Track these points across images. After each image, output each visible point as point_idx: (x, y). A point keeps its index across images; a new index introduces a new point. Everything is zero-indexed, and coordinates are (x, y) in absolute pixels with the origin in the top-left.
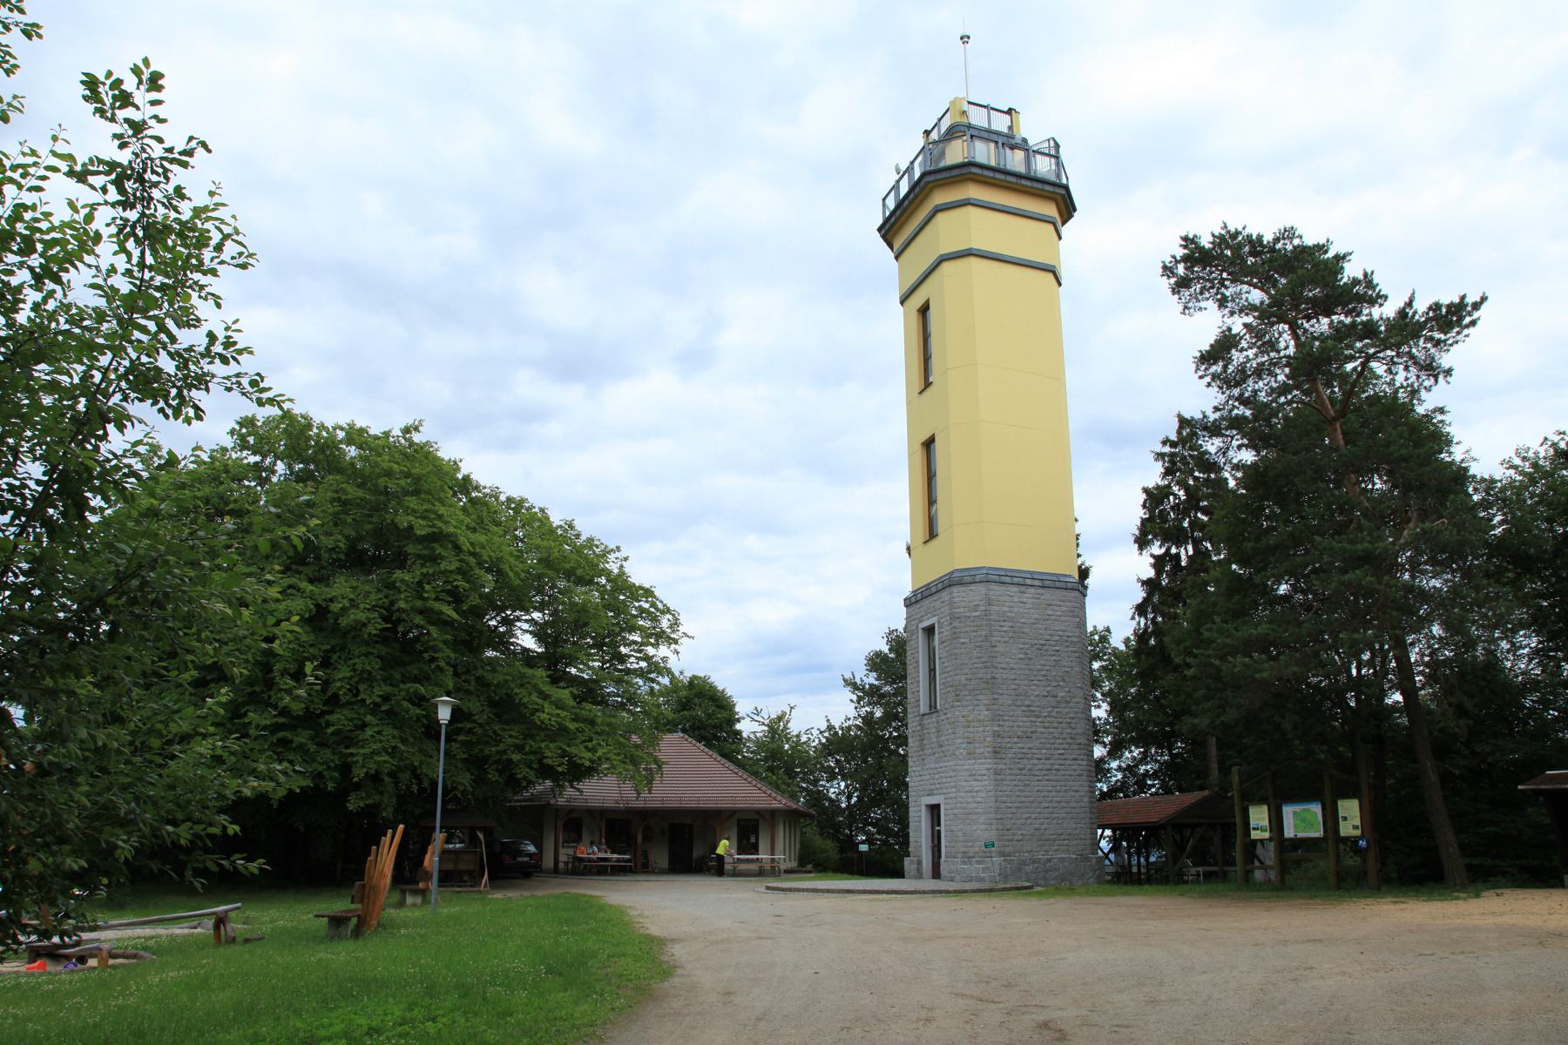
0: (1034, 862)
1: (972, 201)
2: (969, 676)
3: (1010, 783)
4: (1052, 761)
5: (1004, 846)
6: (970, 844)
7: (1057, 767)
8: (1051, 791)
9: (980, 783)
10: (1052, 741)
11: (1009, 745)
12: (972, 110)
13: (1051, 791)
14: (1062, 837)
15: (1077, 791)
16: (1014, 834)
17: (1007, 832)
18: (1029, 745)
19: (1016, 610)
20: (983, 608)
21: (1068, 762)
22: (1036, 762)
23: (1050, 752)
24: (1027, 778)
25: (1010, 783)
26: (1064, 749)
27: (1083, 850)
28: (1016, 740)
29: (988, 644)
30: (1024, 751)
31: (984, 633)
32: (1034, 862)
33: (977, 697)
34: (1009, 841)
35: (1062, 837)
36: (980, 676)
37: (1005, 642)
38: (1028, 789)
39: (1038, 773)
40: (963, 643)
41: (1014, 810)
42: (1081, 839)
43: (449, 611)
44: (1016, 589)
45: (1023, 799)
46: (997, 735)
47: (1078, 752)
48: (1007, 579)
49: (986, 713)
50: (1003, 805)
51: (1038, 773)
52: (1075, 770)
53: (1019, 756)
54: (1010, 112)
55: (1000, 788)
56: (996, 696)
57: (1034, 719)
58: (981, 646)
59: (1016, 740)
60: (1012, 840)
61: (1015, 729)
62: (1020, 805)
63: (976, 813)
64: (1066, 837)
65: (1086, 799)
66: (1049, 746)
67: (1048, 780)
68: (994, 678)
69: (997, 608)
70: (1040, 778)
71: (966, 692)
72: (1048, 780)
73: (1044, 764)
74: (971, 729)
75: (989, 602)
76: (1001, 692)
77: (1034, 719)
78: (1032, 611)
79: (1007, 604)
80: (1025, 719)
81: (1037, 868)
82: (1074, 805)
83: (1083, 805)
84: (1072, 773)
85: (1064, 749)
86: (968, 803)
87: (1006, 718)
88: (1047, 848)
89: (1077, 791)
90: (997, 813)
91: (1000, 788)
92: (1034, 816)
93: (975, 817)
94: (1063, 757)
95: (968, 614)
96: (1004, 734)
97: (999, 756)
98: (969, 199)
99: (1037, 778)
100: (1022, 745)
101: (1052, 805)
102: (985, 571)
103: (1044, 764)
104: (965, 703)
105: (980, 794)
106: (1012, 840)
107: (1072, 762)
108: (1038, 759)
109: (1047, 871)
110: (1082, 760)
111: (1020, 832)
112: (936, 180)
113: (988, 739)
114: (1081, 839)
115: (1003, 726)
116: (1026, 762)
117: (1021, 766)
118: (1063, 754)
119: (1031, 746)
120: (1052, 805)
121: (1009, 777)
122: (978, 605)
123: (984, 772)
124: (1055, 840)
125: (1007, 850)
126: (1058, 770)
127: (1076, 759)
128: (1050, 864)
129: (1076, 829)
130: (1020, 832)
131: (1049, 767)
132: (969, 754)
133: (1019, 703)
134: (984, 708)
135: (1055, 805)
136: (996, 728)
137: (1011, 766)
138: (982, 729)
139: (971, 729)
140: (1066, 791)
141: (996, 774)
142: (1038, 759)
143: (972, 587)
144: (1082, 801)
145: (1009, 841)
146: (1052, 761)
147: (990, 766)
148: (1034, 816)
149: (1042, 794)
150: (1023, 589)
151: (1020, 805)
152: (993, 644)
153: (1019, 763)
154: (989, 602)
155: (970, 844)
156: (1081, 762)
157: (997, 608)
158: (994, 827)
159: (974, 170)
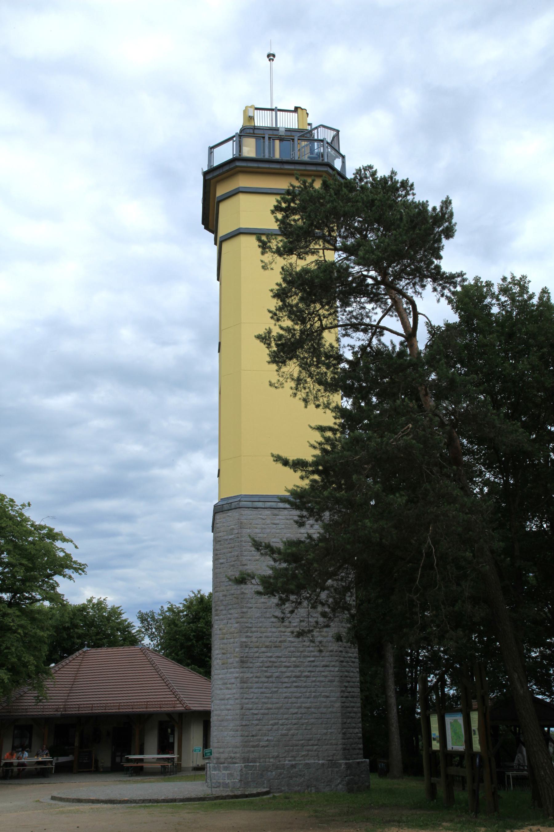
0: (277, 768)
1: (241, 190)
2: (225, 593)
3: (256, 691)
4: (302, 669)
5: (249, 752)
6: (221, 750)
7: (306, 674)
8: (299, 697)
9: (230, 691)
10: (301, 649)
11: (257, 655)
12: (257, 113)
13: (299, 697)
14: (311, 742)
15: (328, 697)
16: (260, 740)
17: (252, 739)
18: (277, 654)
19: (268, 530)
20: (236, 531)
21: (318, 669)
22: (284, 669)
23: (299, 659)
24: (274, 685)
25: (256, 691)
26: (314, 656)
27: (334, 755)
28: (264, 649)
29: (239, 563)
30: (272, 659)
31: (236, 553)
32: (277, 768)
33: (231, 611)
34: (253, 747)
35: (311, 742)
36: (232, 592)
37: (257, 560)
38: (275, 695)
39: (286, 680)
40: (222, 563)
41: (259, 717)
42: (331, 744)
43: (450, 575)
44: (269, 512)
45: (269, 706)
46: (244, 645)
47: (330, 659)
48: (260, 505)
49: (236, 625)
50: (248, 712)
51: (286, 680)
52: (326, 676)
53: (267, 665)
54: (296, 109)
55: (246, 696)
56: (245, 610)
57: (283, 629)
58: (233, 566)
59: (264, 649)
60: (257, 746)
61: (263, 639)
62: (266, 711)
63: (227, 720)
64: (316, 742)
65: (338, 704)
66: (299, 654)
67: (296, 687)
68: (243, 593)
69: (249, 531)
70: (289, 685)
71: (222, 607)
72: (296, 687)
73: (293, 671)
74: (225, 641)
75: (241, 525)
76: (250, 605)
77: (283, 629)
78: (285, 531)
79: (259, 526)
80: (274, 630)
81: (281, 774)
82: (324, 710)
83: (334, 710)
84: (322, 679)
85: (314, 656)
86: (221, 710)
87: (254, 629)
88: (294, 753)
89: (328, 697)
90: (242, 719)
91: (246, 696)
92: (281, 722)
93: (225, 724)
94: (313, 664)
95: (226, 537)
96: (252, 645)
97: (245, 665)
98: (239, 188)
99: (285, 685)
100: (269, 654)
101: (300, 711)
102: (238, 499)
103: (293, 671)
104: (222, 617)
105: (231, 702)
106: (257, 746)
107: (322, 669)
108: (285, 667)
109: (291, 778)
110: (333, 666)
111: (266, 738)
112: (218, 175)
113: (237, 650)
114: (331, 744)
115: (250, 637)
116: (274, 670)
117: (268, 674)
118: (313, 661)
119: (280, 655)
120: (300, 711)
121: (256, 685)
122: (233, 529)
123: (233, 681)
124: (303, 745)
125: (252, 756)
126: (308, 677)
127: (327, 666)
128: (294, 770)
129: (326, 734)
130: (266, 738)
131: (298, 674)
132: (223, 664)
133: (268, 615)
134: (233, 621)
135: (303, 711)
136: (244, 640)
137: (258, 674)
138: (232, 640)
139: (225, 641)
140: (315, 697)
141: (242, 682)
142: (285, 667)
143: (230, 513)
144: (333, 707)
145: (253, 747)
146: (302, 669)
147: (237, 675)
148: (281, 722)
149: (290, 700)
150: (276, 512)
151: (266, 711)
152: (245, 563)
153: (266, 671)
154: (241, 525)
155: (221, 750)
156: (332, 669)
157: (249, 531)
158: (239, 733)
159: (238, 164)
